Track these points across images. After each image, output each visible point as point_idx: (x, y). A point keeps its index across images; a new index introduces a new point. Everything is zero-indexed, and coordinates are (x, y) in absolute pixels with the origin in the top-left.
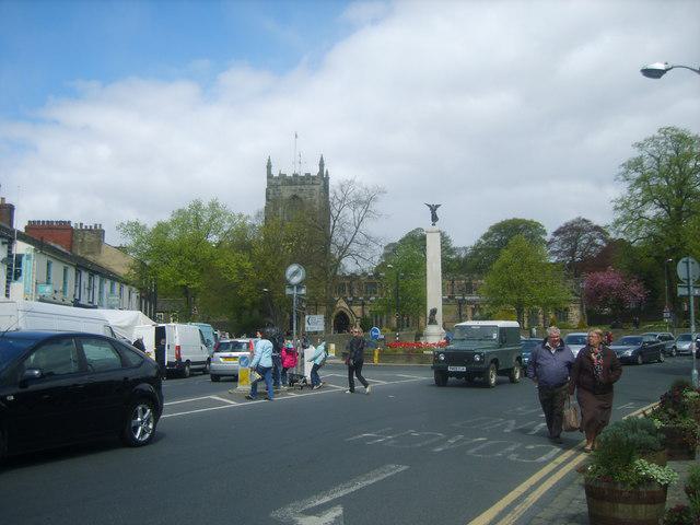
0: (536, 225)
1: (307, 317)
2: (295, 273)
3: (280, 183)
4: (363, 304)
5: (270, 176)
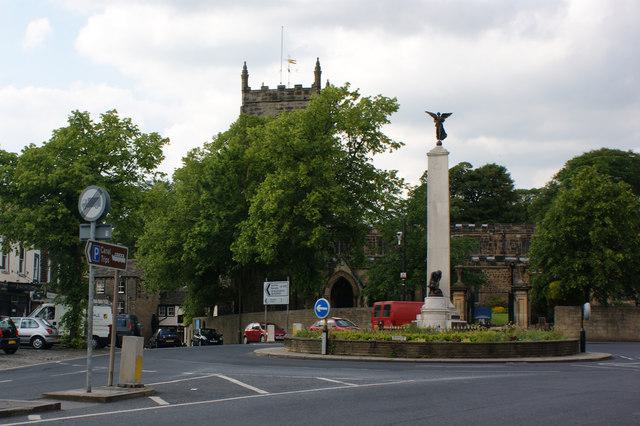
1: (266, 284)
2: (92, 202)
3: (259, 99)
5: (246, 89)
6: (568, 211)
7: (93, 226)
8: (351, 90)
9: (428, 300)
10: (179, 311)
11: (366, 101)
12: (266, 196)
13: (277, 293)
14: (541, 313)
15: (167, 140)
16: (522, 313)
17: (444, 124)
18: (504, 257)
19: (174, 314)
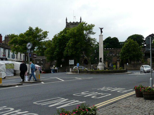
1: (69, 61)
2: (29, 46)
5: (67, 22)
6: (126, 47)
7: (29, 50)
8: (86, 23)
9: (99, 63)
10: (54, 66)
11: (89, 25)
12: (70, 43)
13: (72, 62)
14: (122, 65)
15: (48, 32)
16: (118, 65)
19: (53, 67)
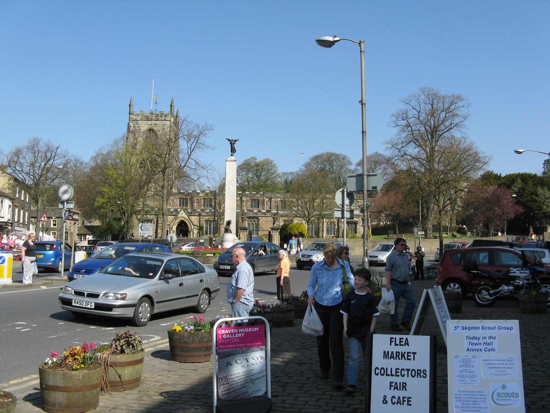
0: (344, 158)
2: (65, 192)
4: (200, 215)
17: (136, 302)
18: (271, 210)
19: (85, 239)
